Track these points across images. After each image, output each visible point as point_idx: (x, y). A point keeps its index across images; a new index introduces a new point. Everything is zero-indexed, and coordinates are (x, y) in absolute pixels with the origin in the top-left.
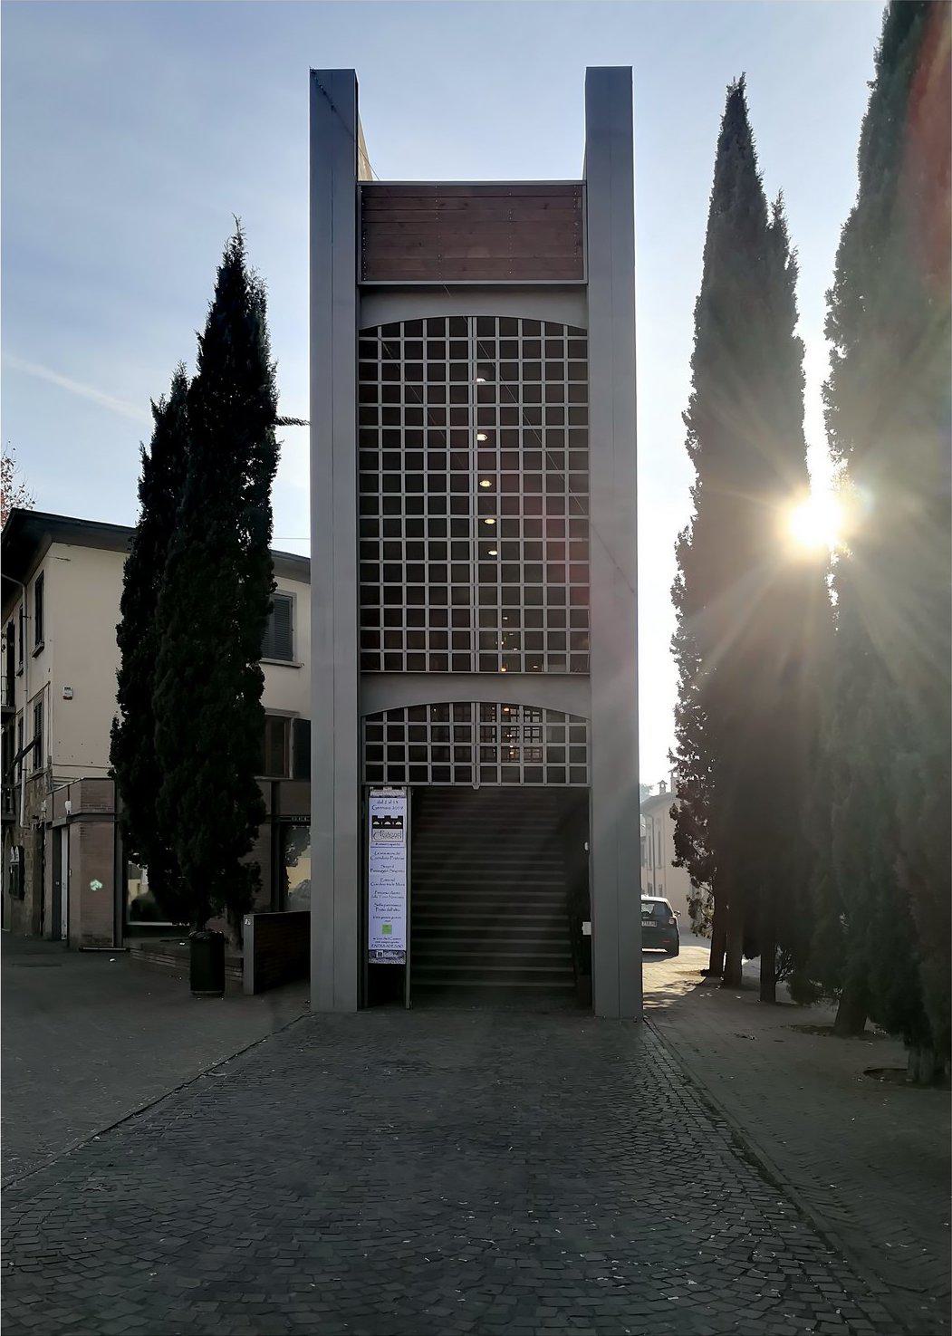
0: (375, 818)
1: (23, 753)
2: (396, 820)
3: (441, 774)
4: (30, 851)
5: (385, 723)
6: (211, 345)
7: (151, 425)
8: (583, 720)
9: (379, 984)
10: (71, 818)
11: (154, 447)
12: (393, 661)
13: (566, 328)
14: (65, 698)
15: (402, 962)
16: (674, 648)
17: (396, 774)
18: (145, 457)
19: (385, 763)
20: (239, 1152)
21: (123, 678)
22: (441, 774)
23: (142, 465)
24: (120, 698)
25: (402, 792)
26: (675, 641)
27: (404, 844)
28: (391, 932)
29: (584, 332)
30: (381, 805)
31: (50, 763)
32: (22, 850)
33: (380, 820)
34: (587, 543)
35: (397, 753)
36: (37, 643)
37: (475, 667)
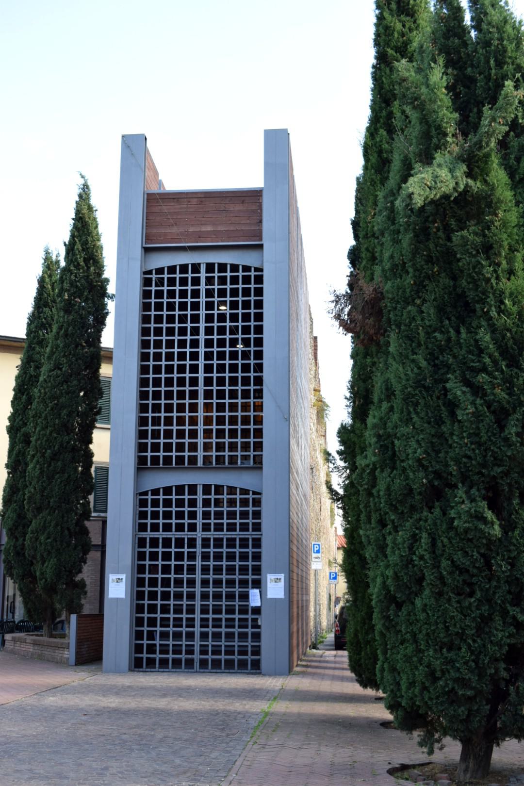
5: (150, 497)
8: (260, 494)
12: (155, 460)
13: (238, 490)
29: (261, 270)
37: (200, 463)
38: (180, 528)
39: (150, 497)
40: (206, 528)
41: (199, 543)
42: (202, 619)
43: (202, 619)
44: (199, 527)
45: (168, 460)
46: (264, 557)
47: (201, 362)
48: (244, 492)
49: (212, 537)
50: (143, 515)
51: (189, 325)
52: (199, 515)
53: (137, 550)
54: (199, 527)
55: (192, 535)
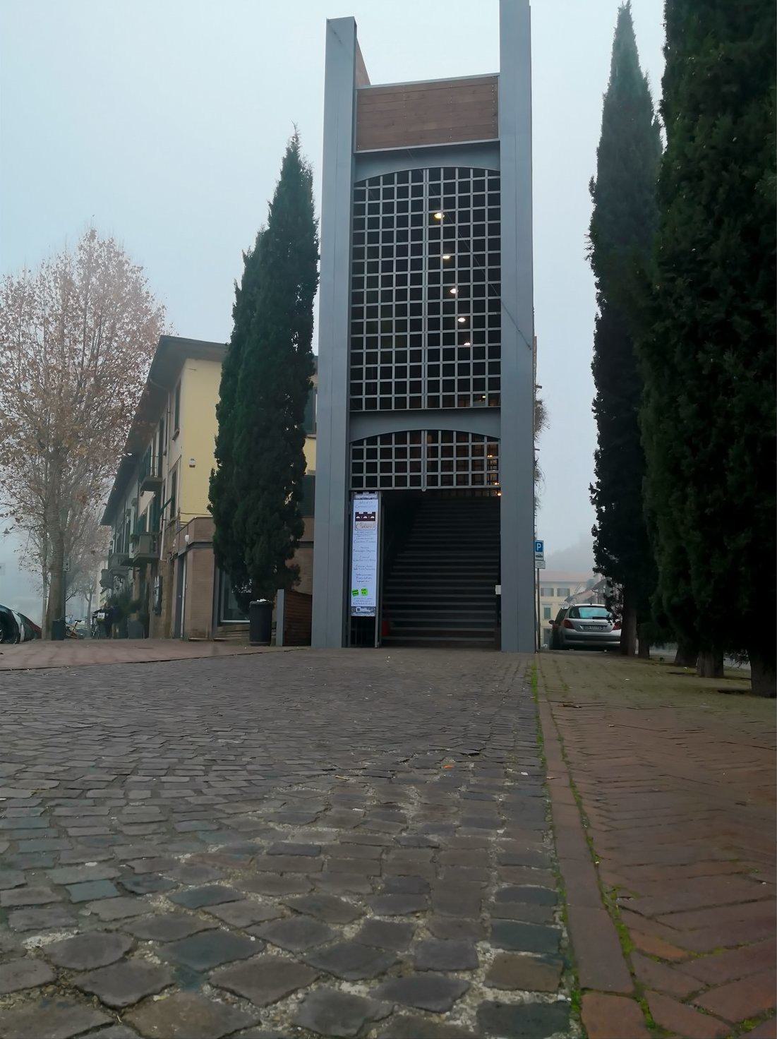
0: (357, 514)
1: (165, 506)
2: (371, 515)
3: (401, 481)
4: (166, 578)
6: (278, 209)
7: (241, 268)
9: (359, 632)
10: (190, 547)
11: (243, 282)
14: (191, 466)
15: (373, 615)
16: (594, 408)
17: (372, 482)
18: (237, 289)
21: (219, 441)
22: (401, 481)
23: (235, 295)
24: (217, 455)
25: (375, 496)
26: (595, 403)
27: (376, 532)
28: (366, 597)
29: (498, 173)
30: (361, 505)
31: (179, 512)
32: (161, 578)
33: (360, 515)
34: (500, 315)
35: (372, 467)
36: (175, 429)
37: (424, 405)
39: (365, 447)
47: (424, 379)
50: (358, 468)
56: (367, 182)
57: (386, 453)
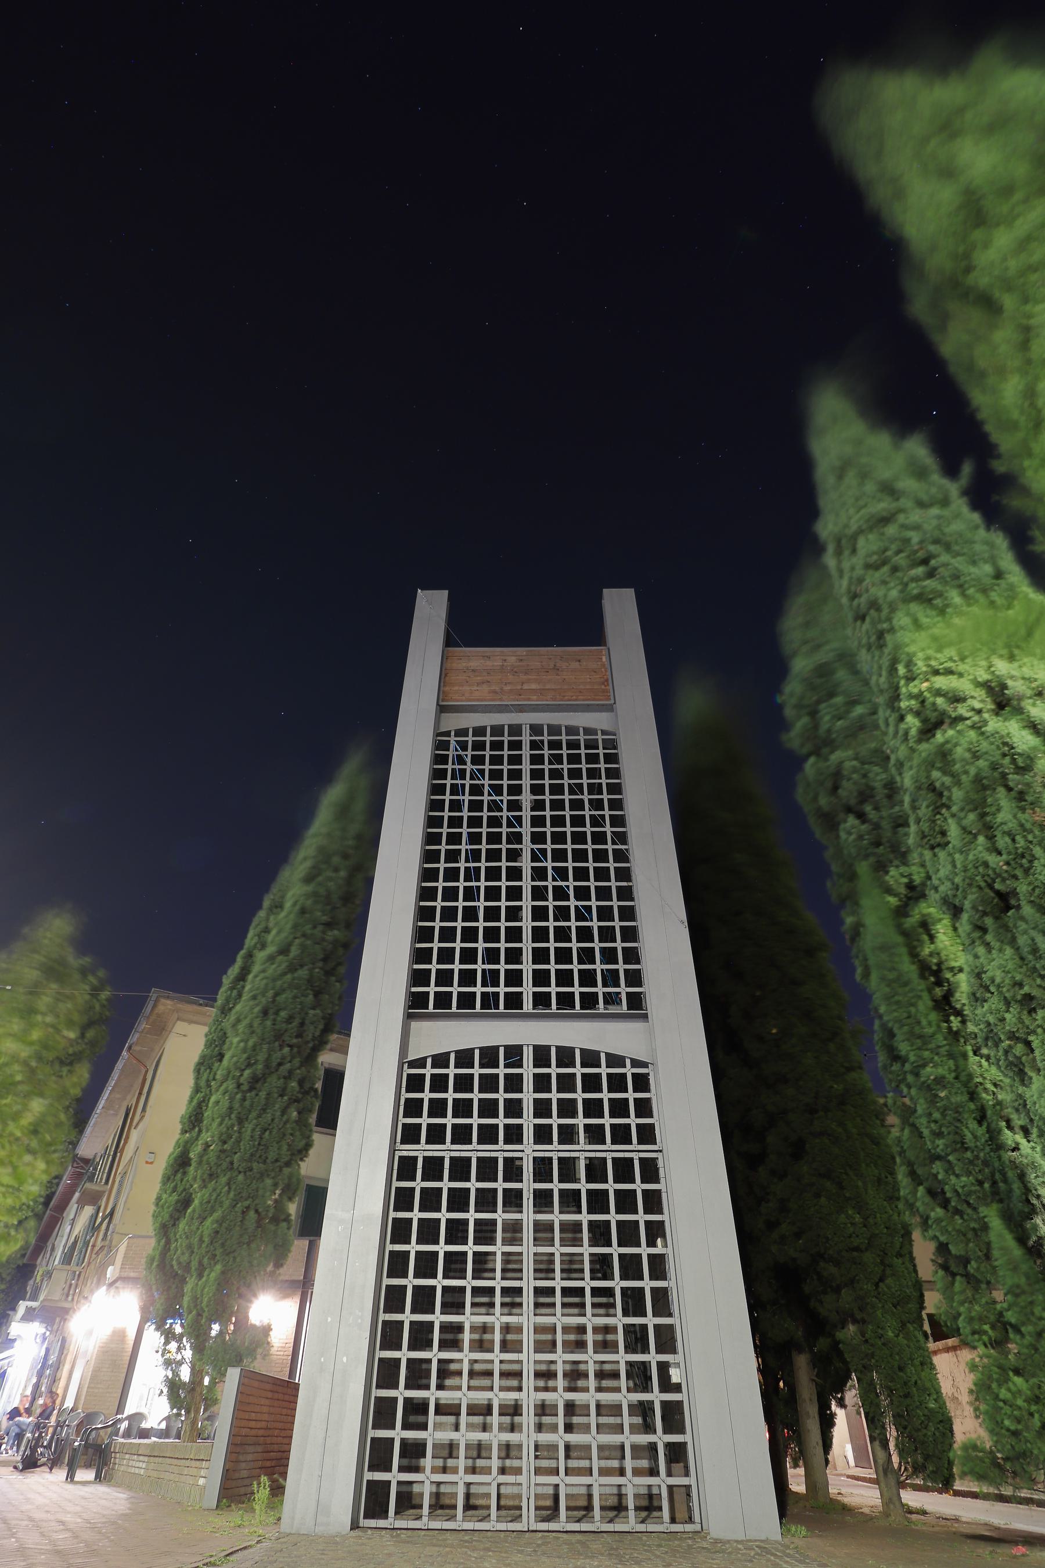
8: (645, 1065)
14: (147, 1162)
19: (418, 1184)
20: (263, 1094)
38: (488, 1135)
39: (428, 1071)
40: (542, 1135)
41: (528, 1170)
42: (538, 1291)
43: (538, 1291)
44: (528, 1134)
45: (466, 1001)
46: (647, 977)
47: (527, 945)
48: (615, 1060)
49: (555, 1156)
51: (502, 967)
52: (528, 978)
53: (405, 1095)
54: (528, 1134)
55: (511, 1150)
56: (429, 1061)
57: (464, 1083)
